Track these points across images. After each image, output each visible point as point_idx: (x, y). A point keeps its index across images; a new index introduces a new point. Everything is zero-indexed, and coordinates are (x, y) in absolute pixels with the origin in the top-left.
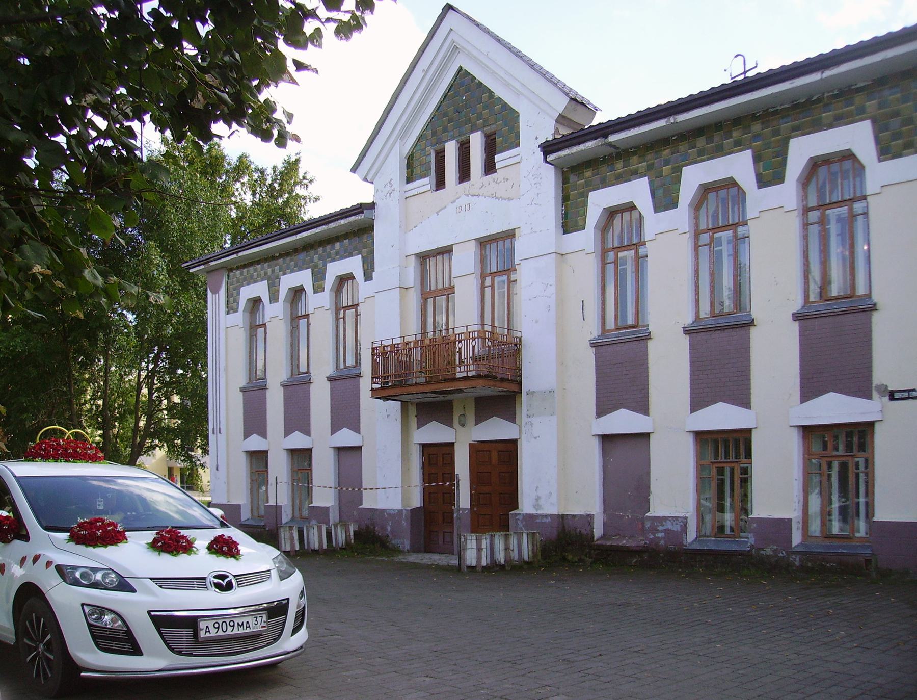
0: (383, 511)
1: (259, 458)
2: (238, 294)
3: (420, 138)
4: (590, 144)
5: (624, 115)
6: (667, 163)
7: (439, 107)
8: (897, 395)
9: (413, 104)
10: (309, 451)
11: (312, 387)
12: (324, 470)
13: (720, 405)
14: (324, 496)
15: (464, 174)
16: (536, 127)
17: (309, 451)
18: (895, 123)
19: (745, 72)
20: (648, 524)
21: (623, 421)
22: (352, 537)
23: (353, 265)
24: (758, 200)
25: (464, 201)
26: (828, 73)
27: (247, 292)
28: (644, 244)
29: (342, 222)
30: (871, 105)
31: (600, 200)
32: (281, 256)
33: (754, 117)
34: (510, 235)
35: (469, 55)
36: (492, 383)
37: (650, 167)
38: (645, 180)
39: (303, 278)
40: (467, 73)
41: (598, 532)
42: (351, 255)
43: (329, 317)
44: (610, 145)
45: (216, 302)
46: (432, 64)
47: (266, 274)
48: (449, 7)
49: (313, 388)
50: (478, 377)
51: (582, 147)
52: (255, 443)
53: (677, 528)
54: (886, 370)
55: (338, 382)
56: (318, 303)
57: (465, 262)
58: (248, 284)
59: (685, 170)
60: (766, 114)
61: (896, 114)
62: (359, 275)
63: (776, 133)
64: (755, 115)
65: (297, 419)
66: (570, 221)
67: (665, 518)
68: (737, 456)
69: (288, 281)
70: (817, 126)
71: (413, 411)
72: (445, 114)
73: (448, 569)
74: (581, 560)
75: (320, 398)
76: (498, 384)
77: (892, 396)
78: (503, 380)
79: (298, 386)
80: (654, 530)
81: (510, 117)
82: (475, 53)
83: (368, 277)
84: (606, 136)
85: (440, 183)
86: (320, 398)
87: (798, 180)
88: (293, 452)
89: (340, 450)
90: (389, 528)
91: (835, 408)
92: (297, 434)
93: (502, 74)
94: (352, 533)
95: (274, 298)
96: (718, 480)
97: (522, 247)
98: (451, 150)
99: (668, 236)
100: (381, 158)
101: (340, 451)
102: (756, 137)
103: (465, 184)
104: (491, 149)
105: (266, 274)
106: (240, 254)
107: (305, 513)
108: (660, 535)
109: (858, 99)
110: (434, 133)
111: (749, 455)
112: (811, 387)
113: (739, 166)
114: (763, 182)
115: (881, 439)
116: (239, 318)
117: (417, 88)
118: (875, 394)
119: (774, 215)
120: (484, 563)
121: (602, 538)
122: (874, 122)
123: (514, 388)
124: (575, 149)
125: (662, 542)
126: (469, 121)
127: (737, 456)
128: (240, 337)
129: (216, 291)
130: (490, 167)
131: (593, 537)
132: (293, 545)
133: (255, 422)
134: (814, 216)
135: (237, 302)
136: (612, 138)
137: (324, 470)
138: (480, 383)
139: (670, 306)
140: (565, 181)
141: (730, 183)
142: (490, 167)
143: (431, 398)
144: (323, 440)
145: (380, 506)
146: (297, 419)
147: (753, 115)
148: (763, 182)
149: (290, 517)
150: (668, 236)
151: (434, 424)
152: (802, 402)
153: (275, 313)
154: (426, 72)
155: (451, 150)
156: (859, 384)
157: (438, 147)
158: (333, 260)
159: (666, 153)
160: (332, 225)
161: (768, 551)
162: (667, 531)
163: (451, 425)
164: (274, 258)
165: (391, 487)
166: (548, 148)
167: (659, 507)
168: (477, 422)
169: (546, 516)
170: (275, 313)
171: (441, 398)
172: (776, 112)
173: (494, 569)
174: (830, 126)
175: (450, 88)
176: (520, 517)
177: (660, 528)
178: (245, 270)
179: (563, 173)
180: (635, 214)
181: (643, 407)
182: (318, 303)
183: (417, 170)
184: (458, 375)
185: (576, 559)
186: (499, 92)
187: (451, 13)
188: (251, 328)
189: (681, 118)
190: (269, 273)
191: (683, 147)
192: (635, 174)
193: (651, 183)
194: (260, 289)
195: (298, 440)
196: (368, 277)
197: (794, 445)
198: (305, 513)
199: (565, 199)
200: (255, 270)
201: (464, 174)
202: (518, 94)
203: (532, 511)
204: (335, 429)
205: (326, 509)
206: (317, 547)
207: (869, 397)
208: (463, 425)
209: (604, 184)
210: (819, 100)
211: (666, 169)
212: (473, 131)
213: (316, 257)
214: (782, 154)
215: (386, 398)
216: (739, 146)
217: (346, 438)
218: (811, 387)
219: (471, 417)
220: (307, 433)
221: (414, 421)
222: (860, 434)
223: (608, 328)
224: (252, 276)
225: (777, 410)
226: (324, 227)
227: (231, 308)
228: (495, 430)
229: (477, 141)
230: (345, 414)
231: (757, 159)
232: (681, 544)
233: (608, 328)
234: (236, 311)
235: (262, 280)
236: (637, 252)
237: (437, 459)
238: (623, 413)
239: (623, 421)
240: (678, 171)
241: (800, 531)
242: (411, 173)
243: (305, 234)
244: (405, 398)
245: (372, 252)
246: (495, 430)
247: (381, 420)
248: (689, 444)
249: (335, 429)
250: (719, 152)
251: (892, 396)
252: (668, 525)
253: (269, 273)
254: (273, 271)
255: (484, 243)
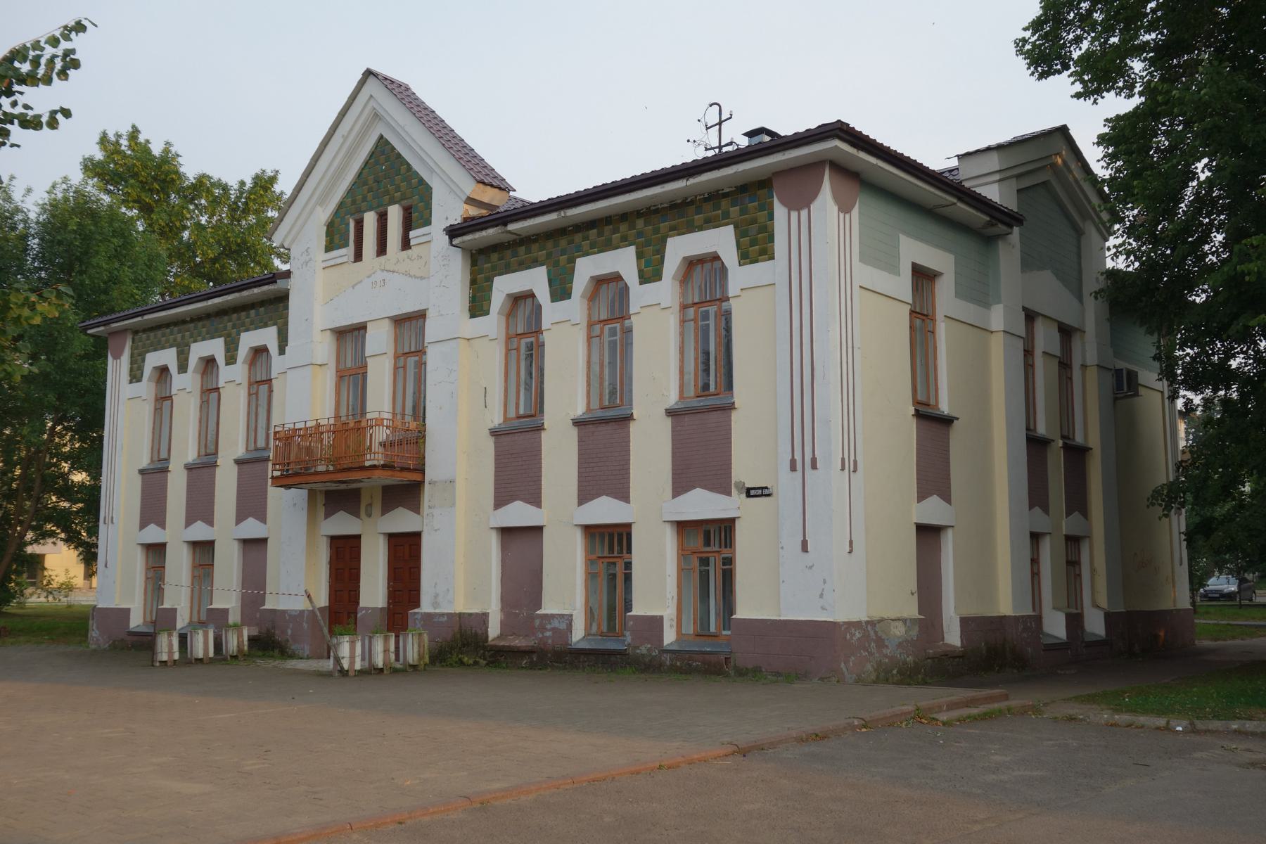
0: (284, 612)
1: (156, 551)
2: (144, 360)
3: (341, 205)
4: (491, 231)
5: (802, 130)
6: (563, 252)
7: (360, 175)
8: (752, 493)
9: (333, 169)
10: (211, 544)
11: (218, 471)
12: (228, 562)
13: (604, 499)
14: (227, 597)
15: (382, 249)
16: (448, 208)
17: (211, 544)
18: (753, 229)
19: (720, 147)
20: (537, 622)
21: (518, 514)
22: (246, 643)
23: (267, 337)
24: (640, 295)
25: (379, 276)
26: (692, 181)
27: (153, 360)
28: (728, 299)
29: (256, 290)
30: (734, 211)
31: (504, 286)
32: (192, 320)
33: (184, 322)
34: (421, 316)
35: (388, 124)
36: (390, 473)
37: (549, 256)
38: (544, 268)
39: (215, 347)
40: (387, 142)
41: (494, 630)
42: (266, 325)
43: (243, 393)
44: (510, 232)
45: (117, 368)
46: (352, 129)
47: (175, 340)
48: (369, 73)
49: (636, 430)
50: (384, 466)
51: (484, 233)
52: (153, 534)
53: (563, 626)
54: (744, 469)
55: (245, 466)
56: (233, 377)
57: (379, 341)
58: (155, 350)
59: (496, 279)
60: (649, 212)
61: (754, 221)
62: (273, 348)
63: (656, 231)
64: (639, 212)
65: (200, 508)
66: (478, 307)
67: (553, 616)
68: (621, 551)
69: (199, 350)
70: (691, 228)
71: (321, 500)
72: (365, 184)
73: (329, 675)
74: (476, 663)
75: (226, 482)
76: (398, 474)
77: (749, 493)
78: (403, 469)
79: (202, 470)
80: (543, 629)
81: (425, 191)
82: (393, 124)
83: (282, 351)
84: (505, 225)
85: (358, 256)
86: (226, 482)
87: (674, 278)
88: (195, 545)
89: (507, 533)
90: (289, 632)
91: (703, 505)
92: (251, 521)
93: (418, 149)
94: (246, 638)
95: (183, 368)
96: (701, 572)
97: (432, 330)
98: (370, 219)
99: (565, 326)
100: (300, 222)
101: (247, 543)
102: (640, 235)
103: (382, 258)
104: (408, 225)
105: (175, 340)
106: (146, 317)
107: (203, 618)
108: (548, 634)
109: (724, 203)
110: (354, 202)
111: (629, 550)
112: (681, 485)
113: (623, 261)
114: (644, 279)
115: (743, 537)
116: (146, 388)
117: (337, 153)
118: (734, 491)
119: (656, 311)
120: (358, 666)
121: (498, 638)
122: (736, 227)
123: (415, 477)
124: (478, 235)
125: (550, 641)
126: (387, 192)
127: (621, 551)
128: (146, 411)
129: (117, 356)
130: (406, 244)
131: (487, 637)
132: (171, 652)
133: (153, 511)
134: (691, 311)
135: (141, 369)
136: (512, 227)
137: (228, 562)
138: (388, 473)
139: (567, 395)
140: (474, 263)
141: (616, 278)
142: (406, 244)
143: (333, 487)
144: (226, 530)
145: (281, 607)
146: (200, 508)
147: (638, 212)
148: (644, 279)
149: (187, 621)
150: (565, 326)
151: (342, 513)
152: (674, 497)
153: (185, 385)
154: (345, 138)
155: (370, 219)
156: (720, 482)
157: (357, 216)
158: (248, 330)
159: (563, 242)
160: (245, 293)
161: (643, 650)
162: (554, 630)
163: (357, 515)
164: (184, 322)
165: (298, 584)
166: (453, 232)
167: (549, 607)
168: (327, 516)
169: (443, 615)
170: (185, 385)
171: (343, 486)
172: (657, 211)
173: (371, 672)
174: (701, 229)
175: (372, 155)
176: (419, 617)
177: (549, 627)
178: (152, 334)
179: (472, 255)
180: (620, 284)
181: (536, 500)
182: (233, 377)
183: (337, 238)
184: (367, 464)
185: (471, 662)
186: (416, 166)
187: (371, 80)
188: (157, 400)
189: (571, 212)
190: (179, 339)
191: (578, 237)
192: (535, 263)
193: (549, 273)
194: (168, 357)
195: (200, 531)
196: (282, 351)
197: (578, 542)
198: (203, 618)
199: (473, 282)
200: (164, 335)
201: (382, 249)
202: (432, 171)
203: (431, 610)
204: (240, 519)
205: (226, 611)
206: (201, 655)
207: (729, 494)
208: (369, 515)
209: (508, 270)
210: (692, 202)
211: (563, 259)
212: (392, 202)
213: (230, 324)
214: (661, 252)
215: (288, 487)
216: (625, 241)
217: (252, 528)
218: (681, 485)
219: (377, 508)
220: (210, 522)
221: (321, 511)
222: (723, 530)
223: (685, 395)
224: (159, 342)
225: (653, 506)
226: (139, 319)
227: (135, 377)
228: (402, 521)
229: (395, 214)
230: (251, 505)
231: (639, 256)
232: (567, 644)
233: (685, 395)
234: (139, 380)
235: (171, 346)
236: (622, 326)
237: (345, 554)
238: (518, 504)
239: (518, 514)
240: (572, 261)
241: (674, 629)
242: (334, 238)
243: (216, 301)
244: (314, 486)
245: (286, 324)
246: (402, 521)
247: (286, 507)
248: (578, 539)
249: (240, 519)
250: (608, 246)
251: (749, 493)
252: (556, 624)
253: (179, 339)
254: (183, 337)
255: (400, 321)
